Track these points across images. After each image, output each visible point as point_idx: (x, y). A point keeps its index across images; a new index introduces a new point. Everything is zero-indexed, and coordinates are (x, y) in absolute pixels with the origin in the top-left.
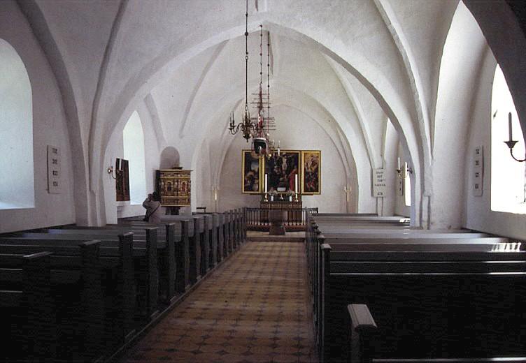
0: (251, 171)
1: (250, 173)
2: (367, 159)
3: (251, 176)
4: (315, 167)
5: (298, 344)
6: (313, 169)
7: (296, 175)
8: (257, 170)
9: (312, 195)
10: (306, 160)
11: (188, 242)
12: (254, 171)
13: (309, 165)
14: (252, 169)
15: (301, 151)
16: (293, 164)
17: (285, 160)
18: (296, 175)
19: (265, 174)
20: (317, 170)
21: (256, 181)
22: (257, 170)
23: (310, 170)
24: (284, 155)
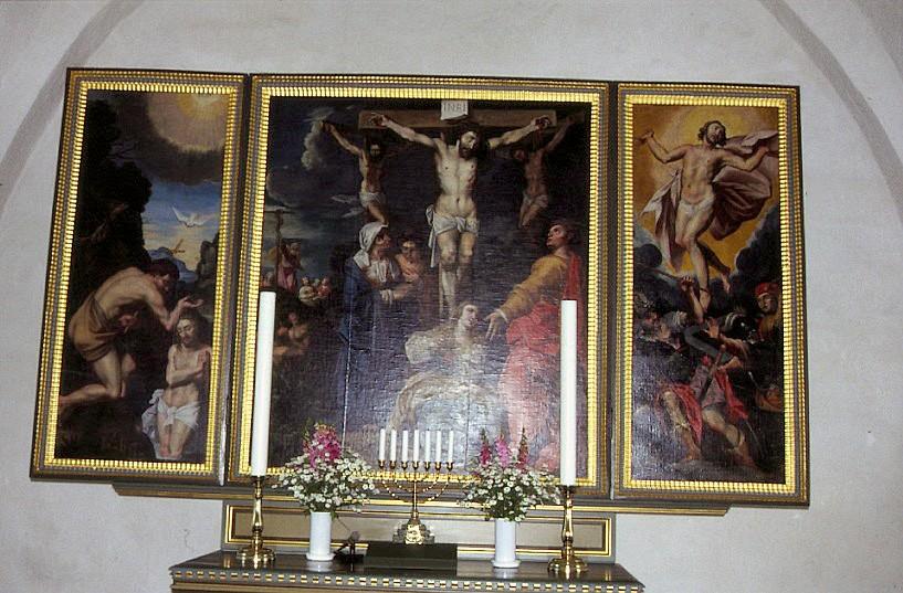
0: (145, 263)
1: (131, 285)
2: (470, 563)
3: (139, 306)
4: (748, 235)
5: (147, 222)
6: (729, 252)
7: (569, 309)
8: (190, 259)
9: (720, 504)
10: (662, 176)
11: (787, 479)
12: (164, 266)
13: (693, 213)
14: (151, 243)
15: (613, 91)
16: (534, 202)
17: (455, 173)
18: (569, 309)
19: (262, 289)
20: (762, 264)
21: (180, 363)
22: (190, 259)
23: (693, 267)
24: (453, 131)
